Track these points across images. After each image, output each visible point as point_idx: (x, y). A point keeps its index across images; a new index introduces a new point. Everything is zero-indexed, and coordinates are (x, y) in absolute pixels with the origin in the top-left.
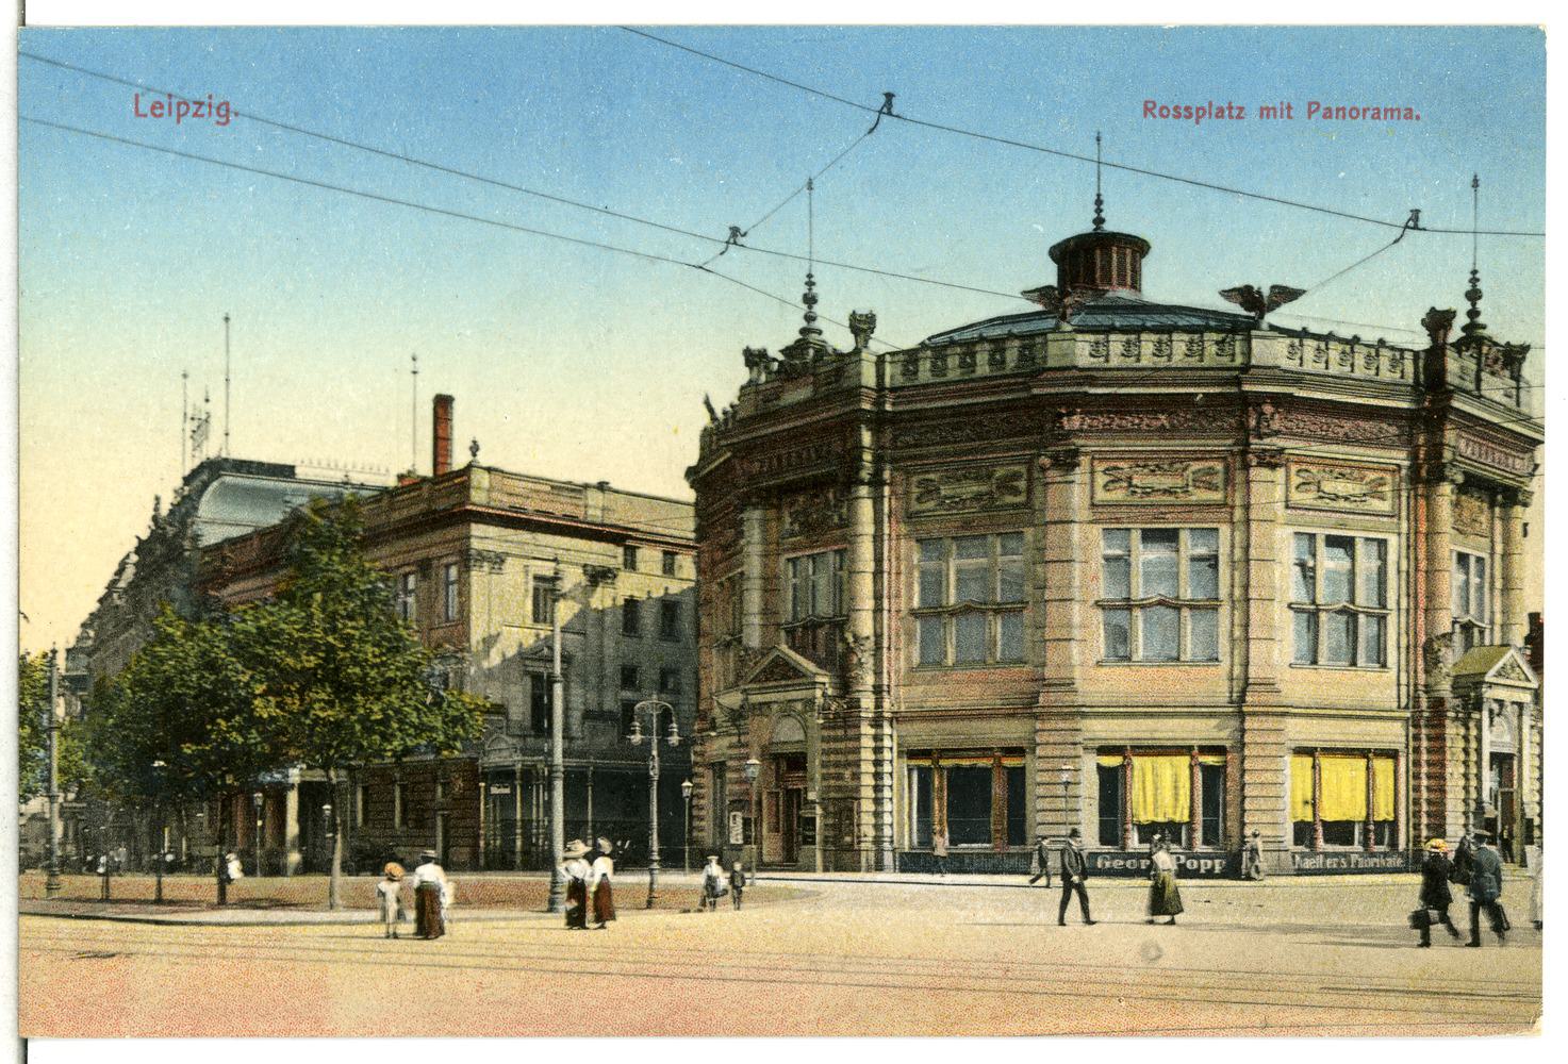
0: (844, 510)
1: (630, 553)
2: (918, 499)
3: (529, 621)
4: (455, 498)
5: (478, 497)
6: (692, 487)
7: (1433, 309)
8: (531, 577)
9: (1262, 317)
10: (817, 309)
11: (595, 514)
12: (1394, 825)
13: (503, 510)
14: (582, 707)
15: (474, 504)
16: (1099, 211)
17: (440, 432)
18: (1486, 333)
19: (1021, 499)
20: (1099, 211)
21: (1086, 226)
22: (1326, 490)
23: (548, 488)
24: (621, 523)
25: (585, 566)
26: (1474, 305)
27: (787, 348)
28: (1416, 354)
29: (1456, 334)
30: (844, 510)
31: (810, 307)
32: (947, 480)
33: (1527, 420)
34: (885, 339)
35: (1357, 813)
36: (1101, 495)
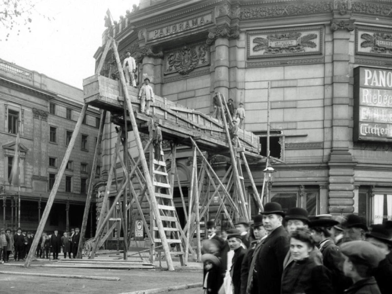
0: (206, 57)
2: (254, 49)
3: (7, 131)
6: (260, 143)
14: (31, 174)
17: (232, 58)
19: (316, 49)
22: (378, 45)
24: (12, 137)
25: (33, 108)
30: (206, 57)
32: (271, 38)
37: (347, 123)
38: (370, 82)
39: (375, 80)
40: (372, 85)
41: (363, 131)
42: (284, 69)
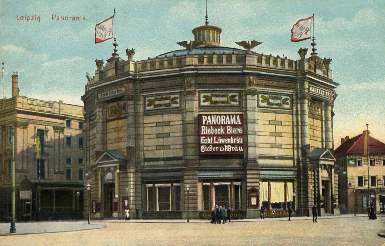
1: (69, 123)
4: (12, 107)
5: (19, 106)
7: (301, 48)
8: (36, 130)
9: (249, 50)
10: (315, 47)
11: (57, 111)
12: (293, 202)
13: (27, 109)
15: (18, 108)
16: (207, 20)
18: (318, 55)
20: (207, 20)
21: (204, 24)
23: (43, 103)
26: (314, 47)
27: (108, 60)
28: (296, 62)
29: (308, 55)
31: (115, 47)
33: (330, 81)
34: (137, 57)
35: (282, 201)
36: (202, 104)
37: (194, 145)
38: (206, 122)
39: (209, 121)
40: (207, 124)
41: (203, 150)
42: (163, 117)
